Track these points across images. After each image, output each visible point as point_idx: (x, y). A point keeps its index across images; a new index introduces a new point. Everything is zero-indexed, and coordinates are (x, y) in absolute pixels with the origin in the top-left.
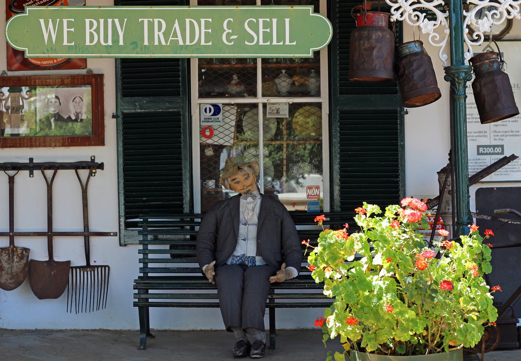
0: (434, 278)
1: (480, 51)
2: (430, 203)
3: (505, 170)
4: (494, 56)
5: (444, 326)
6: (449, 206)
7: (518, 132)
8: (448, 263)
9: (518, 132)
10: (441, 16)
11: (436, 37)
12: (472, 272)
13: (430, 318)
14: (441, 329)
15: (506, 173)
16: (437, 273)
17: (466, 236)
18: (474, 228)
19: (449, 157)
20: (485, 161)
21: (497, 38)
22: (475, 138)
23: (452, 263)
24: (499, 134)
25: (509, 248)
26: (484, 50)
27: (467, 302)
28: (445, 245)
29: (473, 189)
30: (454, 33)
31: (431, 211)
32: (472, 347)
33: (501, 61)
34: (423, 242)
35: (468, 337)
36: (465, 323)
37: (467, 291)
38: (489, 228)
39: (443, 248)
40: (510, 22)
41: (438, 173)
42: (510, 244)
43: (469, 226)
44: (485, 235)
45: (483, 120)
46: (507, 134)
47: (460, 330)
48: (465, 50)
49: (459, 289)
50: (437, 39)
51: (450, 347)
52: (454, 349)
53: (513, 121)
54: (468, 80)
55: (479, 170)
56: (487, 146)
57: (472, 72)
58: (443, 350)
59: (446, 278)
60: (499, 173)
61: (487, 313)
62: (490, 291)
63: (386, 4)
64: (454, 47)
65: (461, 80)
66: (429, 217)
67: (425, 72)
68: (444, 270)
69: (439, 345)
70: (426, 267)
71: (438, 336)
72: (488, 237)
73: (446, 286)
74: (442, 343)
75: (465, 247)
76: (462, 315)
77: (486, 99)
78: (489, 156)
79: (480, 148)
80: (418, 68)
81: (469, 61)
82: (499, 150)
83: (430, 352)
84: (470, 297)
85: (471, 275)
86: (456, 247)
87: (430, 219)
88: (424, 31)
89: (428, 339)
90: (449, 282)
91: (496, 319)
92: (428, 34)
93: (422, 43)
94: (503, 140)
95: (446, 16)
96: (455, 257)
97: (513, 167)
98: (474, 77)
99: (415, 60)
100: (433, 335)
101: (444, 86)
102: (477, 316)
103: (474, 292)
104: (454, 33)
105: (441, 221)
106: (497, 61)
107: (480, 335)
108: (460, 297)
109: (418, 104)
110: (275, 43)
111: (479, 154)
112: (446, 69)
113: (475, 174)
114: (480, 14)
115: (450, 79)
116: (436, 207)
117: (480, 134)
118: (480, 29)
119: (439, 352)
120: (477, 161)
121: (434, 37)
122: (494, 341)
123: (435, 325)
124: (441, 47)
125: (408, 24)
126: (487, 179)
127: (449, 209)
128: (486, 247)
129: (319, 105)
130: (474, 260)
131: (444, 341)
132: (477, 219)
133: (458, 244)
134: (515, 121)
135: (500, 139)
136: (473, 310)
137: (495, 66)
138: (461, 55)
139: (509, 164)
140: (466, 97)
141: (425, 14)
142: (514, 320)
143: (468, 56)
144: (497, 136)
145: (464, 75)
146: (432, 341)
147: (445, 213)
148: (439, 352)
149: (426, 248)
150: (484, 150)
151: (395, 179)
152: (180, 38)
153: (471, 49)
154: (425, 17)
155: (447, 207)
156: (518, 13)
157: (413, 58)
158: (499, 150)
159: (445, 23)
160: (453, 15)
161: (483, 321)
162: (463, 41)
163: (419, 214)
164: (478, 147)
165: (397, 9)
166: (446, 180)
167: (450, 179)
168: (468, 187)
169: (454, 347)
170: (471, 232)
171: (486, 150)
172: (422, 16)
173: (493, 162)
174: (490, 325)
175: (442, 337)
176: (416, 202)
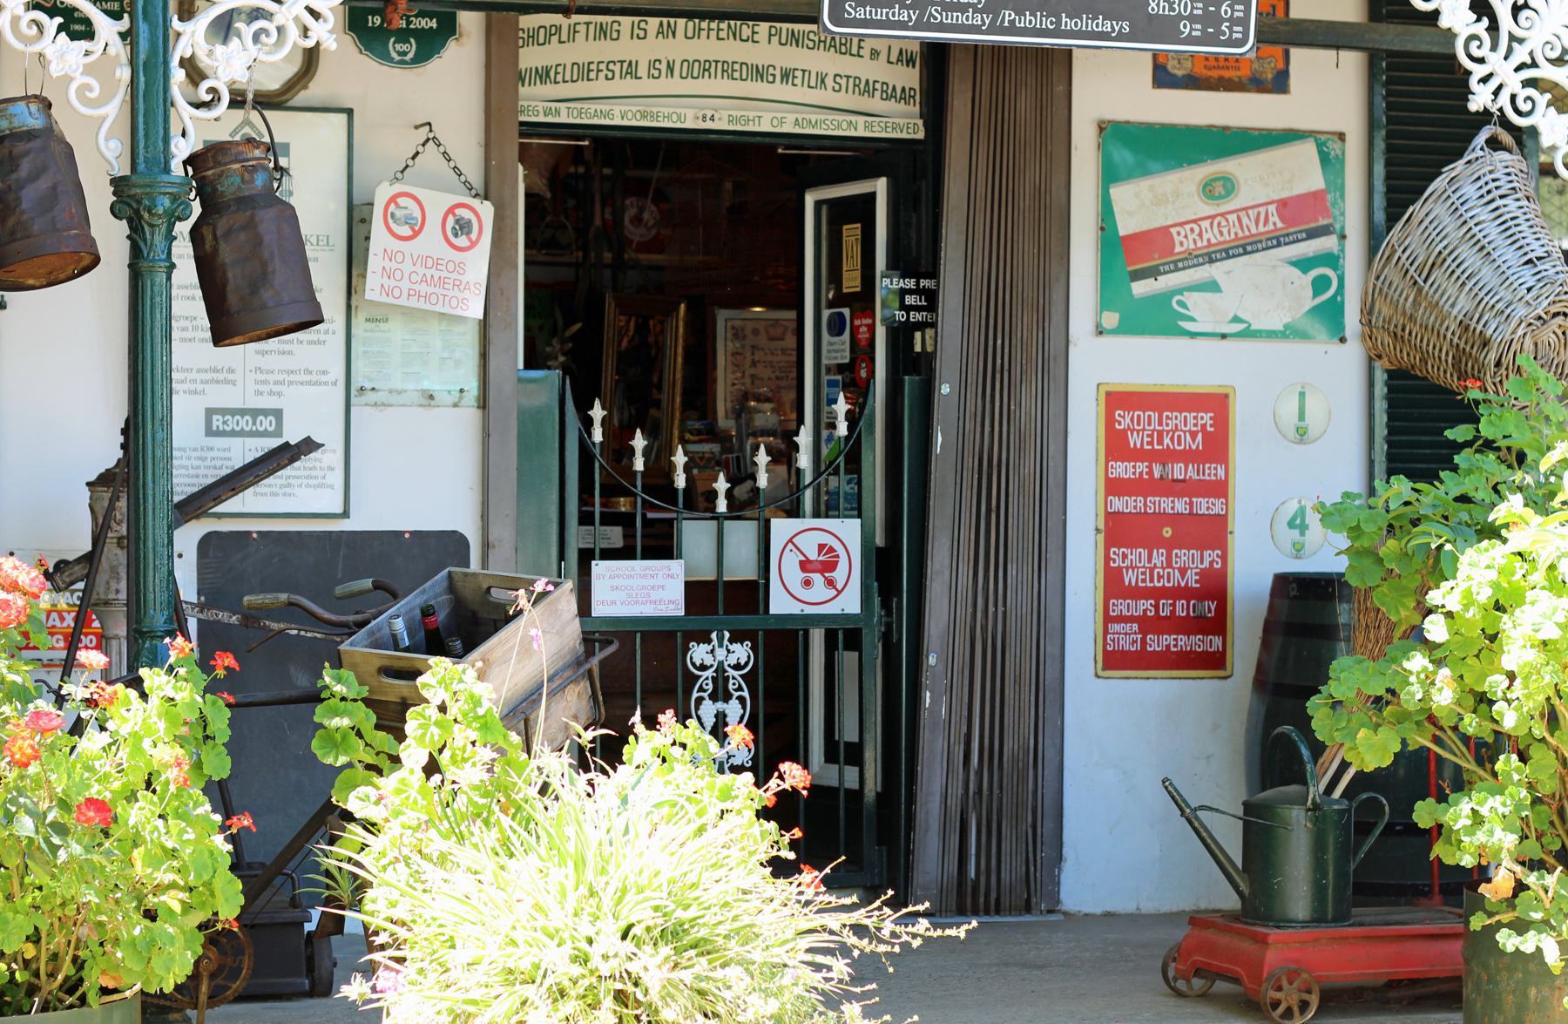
0: (59, 790)
1: (221, 134)
2: (58, 574)
3: (283, 482)
4: (257, 153)
5: (83, 931)
6: (119, 581)
7: (324, 373)
8: (104, 749)
9: (324, 373)
10: (107, 29)
11: (91, 90)
12: (172, 774)
13: (47, 907)
14: (78, 940)
15: (288, 490)
16: (69, 777)
17: (156, 670)
18: (180, 648)
19: (121, 439)
20: (227, 454)
21: (267, 102)
22: (200, 387)
23: (114, 748)
24: (271, 378)
25: (292, 706)
26: (235, 132)
27: (154, 862)
28: (96, 696)
29: (188, 538)
30: (142, 79)
31: (68, 594)
32: (166, 991)
33: (277, 168)
34: (30, 685)
35: (156, 962)
36: (147, 922)
37: (156, 828)
38: (225, 650)
39: (90, 703)
40: (311, 57)
41: (88, 484)
42: (288, 693)
43: (167, 640)
44: (214, 668)
45: (221, 335)
46: (292, 377)
47: (133, 943)
48: (175, 130)
49: (131, 823)
51: (105, 991)
52: (116, 997)
53: (310, 343)
54: (180, 219)
55: (210, 481)
56: (234, 412)
57: (192, 195)
58: (83, 1000)
59: (94, 791)
60: (268, 490)
61: (212, 895)
62: (223, 828)
63: (1454, 57)
64: (141, 119)
65: (160, 217)
66: (60, 613)
67: (54, 188)
68: (90, 769)
69: (72, 986)
70: (36, 758)
71: (68, 959)
72: (221, 673)
73: (92, 814)
74: (81, 980)
75: (154, 700)
76: (140, 899)
77: (230, 275)
78: (238, 441)
79: (215, 417)
80: (33, 178)
81: (185, 163)
82: (267, 423)
83: (45, 1008)
84: (163, 848)
85: (167, 783)
86: (128, 700)
87: (62, 619)
88: (55, 70)
89: (38, 969)
90: (103, 803)
91: (238, 911)
92: (68, 79)
93: (50, 105)
94: (279, 394)
95: (123, 30)
96: (124, 730)
97: (307, 473)
98: (197, 209)
99: (27, 153)
100: (55, 957)
101: (110, 235)
102: (182, 902)
103: (174, 831)
104: (142, 79)
105: (96, 624)
106: (265, 168)
107: (190, 958)
108: (136, 845)
109: (31, 282)
111: (210, 432)
112: (118, 183)
113: (196, 489)
114: (224, 27)
115: (129, 212)
116: (81, 585)
117: (215, 376)
118: (220, 71)
119: (71, 1007)
120: (204, 454)
122: (234, 974)
123: (61, 928)
124: (104, 119)
125: (10, 46)
126: (231, 505)
127: (117, 591)
128: (214, 703)
130: (180, 740)
131: (84, 974)
132: (199, 620)
133: (133, 694)
134: (319, 342)
135: (271, 393)
136: (173, 886)
137: (260, 180)
138: (161, 144)
139: (296, 464)
140: (173, 266)
141: (59, 20)
142: (291, 915)
143: (181, 149)
144: (265, 382)
145: (167, 202)
146: (52, 975)
147: (107, 603)
148: (71, 1007)
149: (39, 702)
150: (225, 423)
153: (191, 130)
154: (60, 29)
155: (114, 586)
156: (331, 32)
157: (21, 147)
158: (267, 423)
159: (119, 50)
160: (143, 28)
161: (201, 916)
162: (168, 103)
163: (20, 603)
164: (210, 412)
166: (111, 507)
167: (122, 504)
168: (171, 528)
169: (115, 991)
170: (172, 660)
171: (233, 423)
172: (1542, 99)
173: (249, 458)
174: (219, 927)
175: (78, 963)
176: (16, 568)
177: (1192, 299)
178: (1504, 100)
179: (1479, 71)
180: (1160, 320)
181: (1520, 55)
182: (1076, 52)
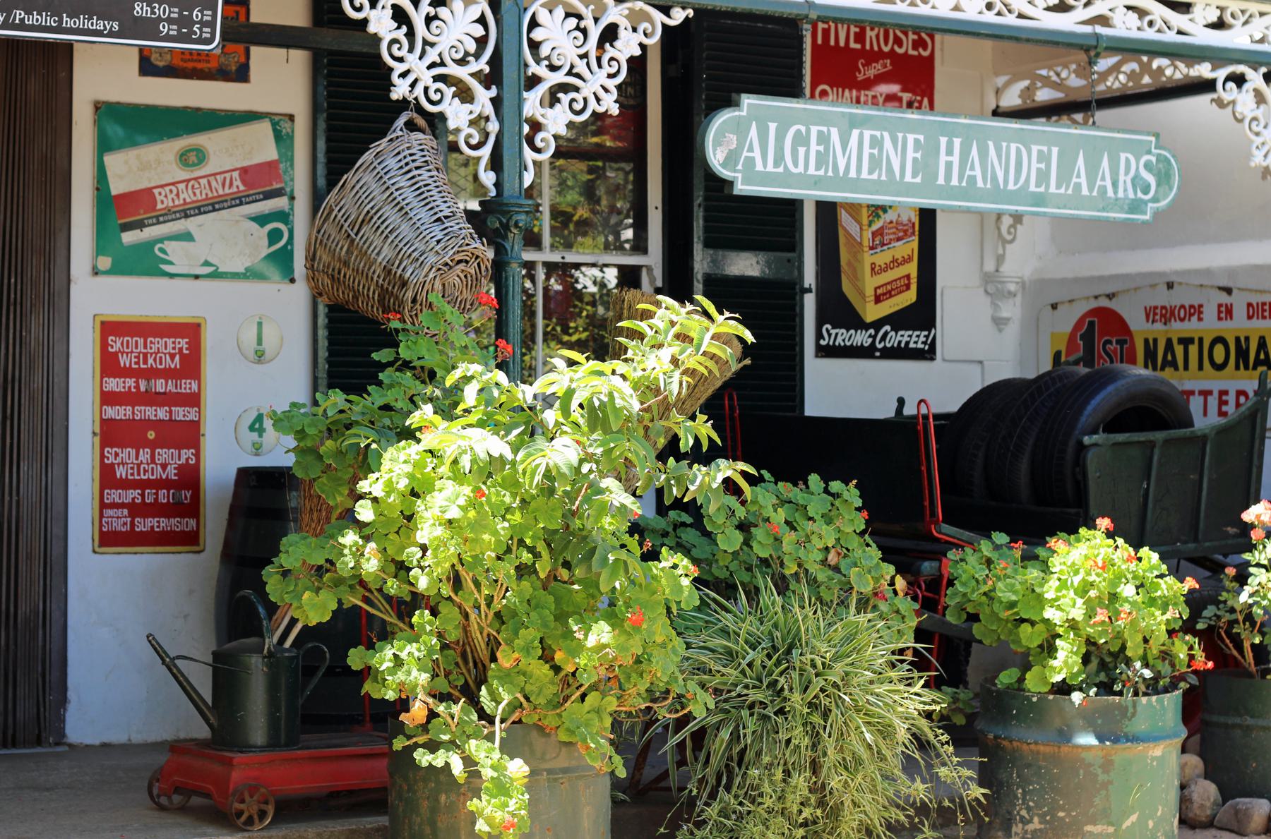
50: (474, 141)
110: (1053, 189)
121: (470, 136)
141: (454, 89)
151: (180, 413)
165: (404, 75)
177: (170, 246)
178: (419, 91)
179: (399, 68)
180: (144, 263)
181: (432, 56)
182: (76, 46)
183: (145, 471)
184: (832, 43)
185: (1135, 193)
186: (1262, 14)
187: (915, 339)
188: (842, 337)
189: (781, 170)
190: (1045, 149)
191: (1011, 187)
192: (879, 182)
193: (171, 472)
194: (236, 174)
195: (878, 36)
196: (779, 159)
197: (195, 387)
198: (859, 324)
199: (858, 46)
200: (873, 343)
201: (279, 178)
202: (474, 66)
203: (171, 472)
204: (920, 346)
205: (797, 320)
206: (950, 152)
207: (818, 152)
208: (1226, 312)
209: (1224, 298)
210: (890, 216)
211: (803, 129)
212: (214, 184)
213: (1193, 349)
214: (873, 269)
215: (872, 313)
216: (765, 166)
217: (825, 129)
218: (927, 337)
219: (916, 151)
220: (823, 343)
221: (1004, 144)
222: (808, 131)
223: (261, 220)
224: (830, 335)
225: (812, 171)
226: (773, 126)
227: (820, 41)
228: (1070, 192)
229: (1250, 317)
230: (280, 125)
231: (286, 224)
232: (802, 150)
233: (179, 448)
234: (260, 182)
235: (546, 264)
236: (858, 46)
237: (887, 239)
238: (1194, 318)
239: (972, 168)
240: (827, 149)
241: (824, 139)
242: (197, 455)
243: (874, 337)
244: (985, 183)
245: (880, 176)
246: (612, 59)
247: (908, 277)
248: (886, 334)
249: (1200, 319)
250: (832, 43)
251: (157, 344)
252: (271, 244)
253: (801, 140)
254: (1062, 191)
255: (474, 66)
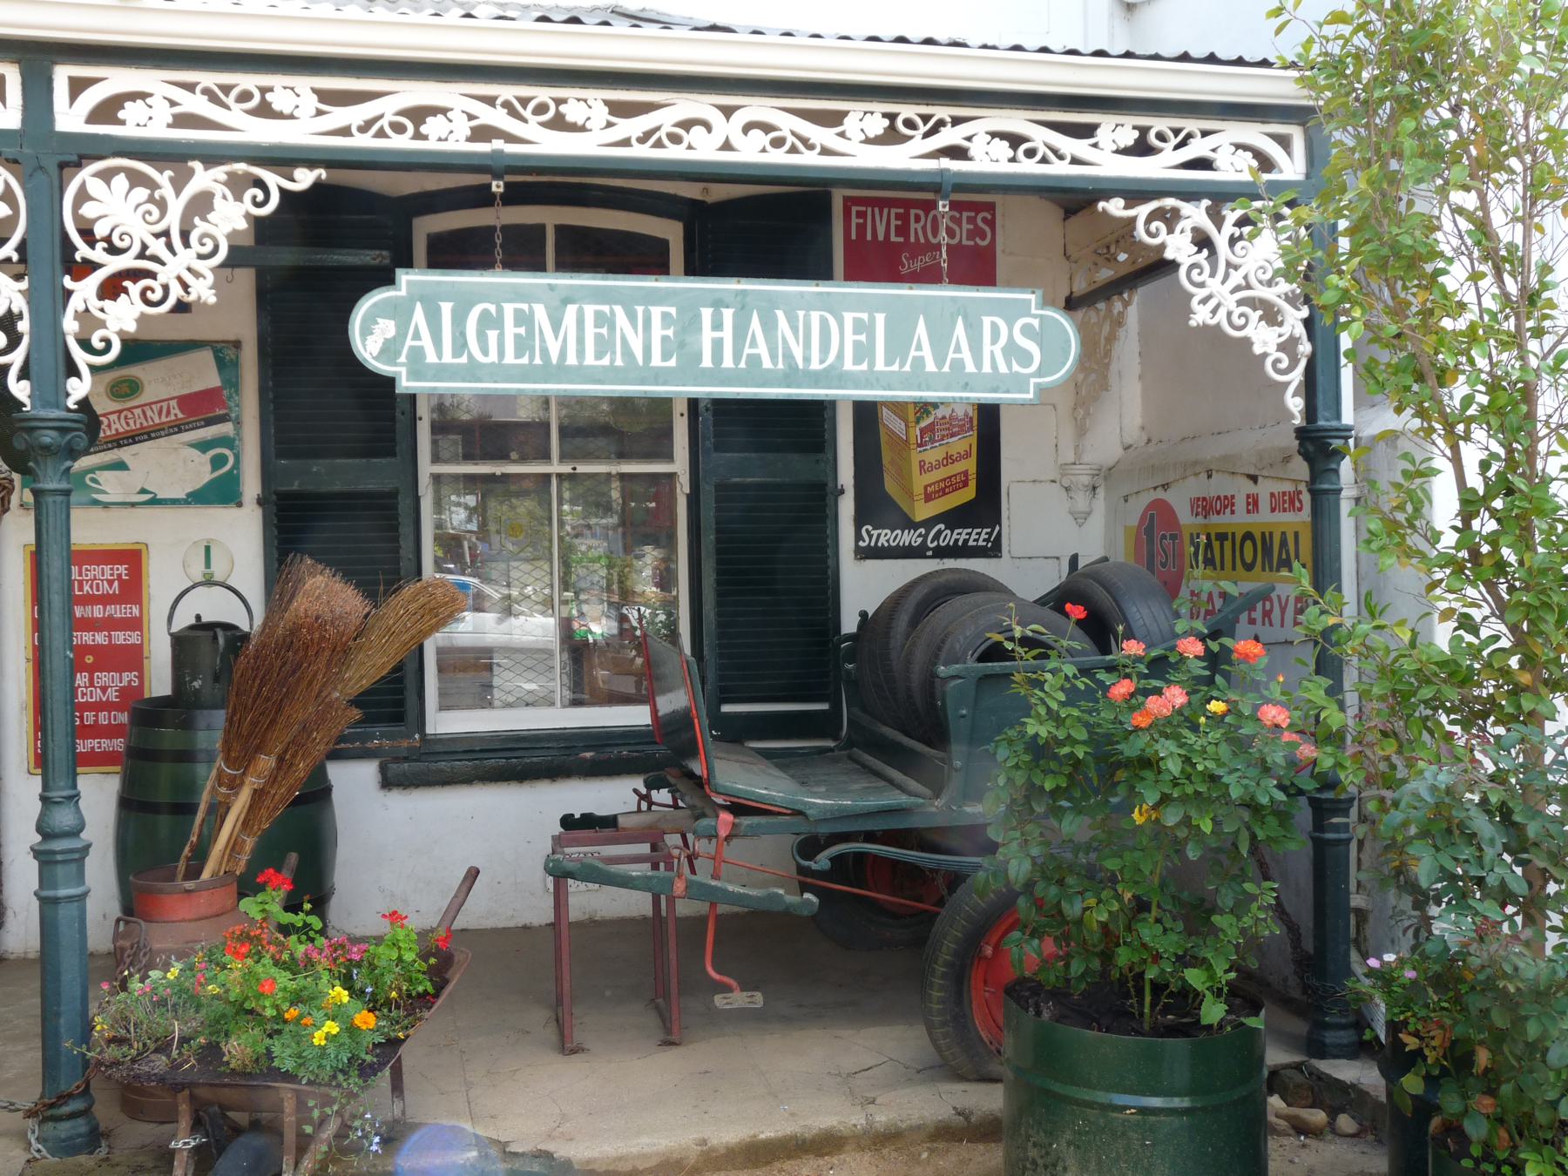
110: (880, 366)
124: (1288, 384)
129: (671, 476)
151: (120, 637)
152: (966, 355)
154: (204, 219)
165: (1204, 301)
172: (1255, 316)
177: (103, 476)
178: (1221, 315)
181: (1236, 278)
183: (83, 694)
184: (869, 237)
185: (1010, 367)
186: (1205, 134)
187: (977, 536)
188: (885, 537)
189: (464, 360)
190: (865, 316)
191: (815, 365)
192: (612, 367)
193: (112, 695)
194: (173, 403)
195: (924, 228)
196: (460, 345)
197: (136, 611)
198: (910, 525)
199: (901, 240)
200: (924, 541)
201: (223, 405)
202: (167, 191)
203: (112, 695)
204: (981, 543)
205: (829, 522)
206: (717, 325)
207: (517, 336)
208: (1253, 503)
209: (1250, 488)
210: (940, 413)
211: (492, 308)
212: (149, 413)
213: (1228, 544)
214: (921, 467)
215: (923, 511)
216: (439, 354)
217: (525, 307)
218: (990, 534)
219: (665, 326)
220: (861, 544)
221: (801, 314)
222: (500, 311)
223: (203, 446)
224: (870, 536)
225: (510, 359)
226: (446, 308)
227: (854, 237)
228: (907, 368)
229: (1273, 510)
230: (225, 354)
231: (231, 449)
232: (492, 335)
233: (120, 671)
234: (200, 408)
235: (559, 476)
236: (901, 240)
237: (938, 435)
238: (1228, 511)
239: (754, 344)
240: (530, 331)
241: (524, 319)
242: (141, 678)
243: (925, 537)
244: (775, 363)
245: (612, 361)
246: (205, 235)
247: (966, 473)
248: (939, 532)
249: (1233, 512)
250: (869, 237)
251: (94, 571)
252: (214, 469)
253: (487, 321)
254: (895, 367)
255: (167, 191)
